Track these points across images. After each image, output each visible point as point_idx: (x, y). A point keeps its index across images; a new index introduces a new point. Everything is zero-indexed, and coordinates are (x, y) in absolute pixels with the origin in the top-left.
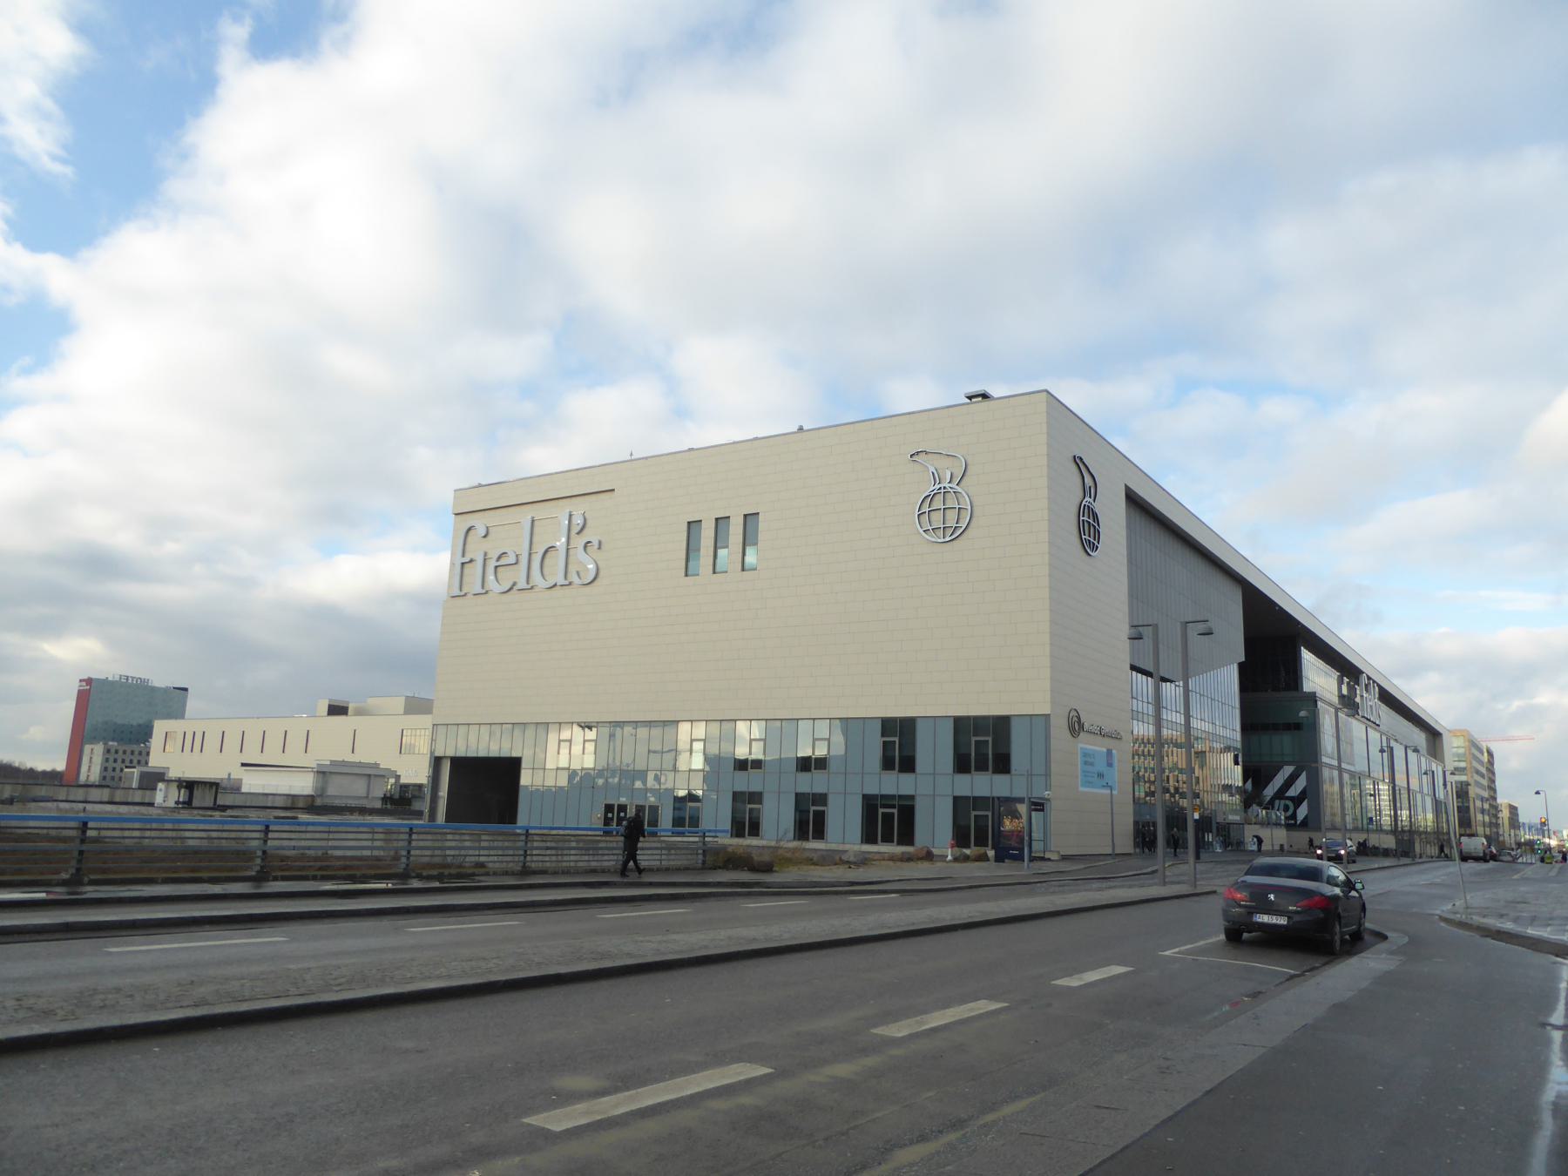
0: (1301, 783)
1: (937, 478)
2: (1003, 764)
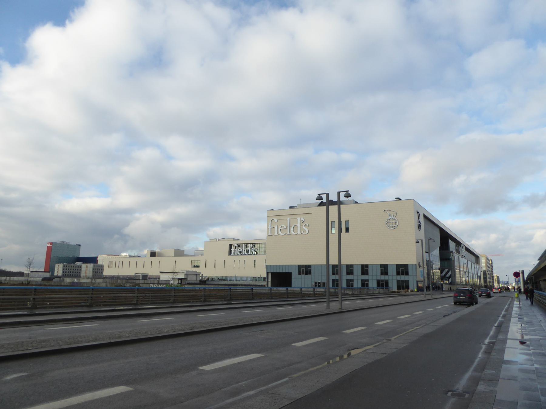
0: (450, 273)
1: (390, 216)
2: (407, 274)
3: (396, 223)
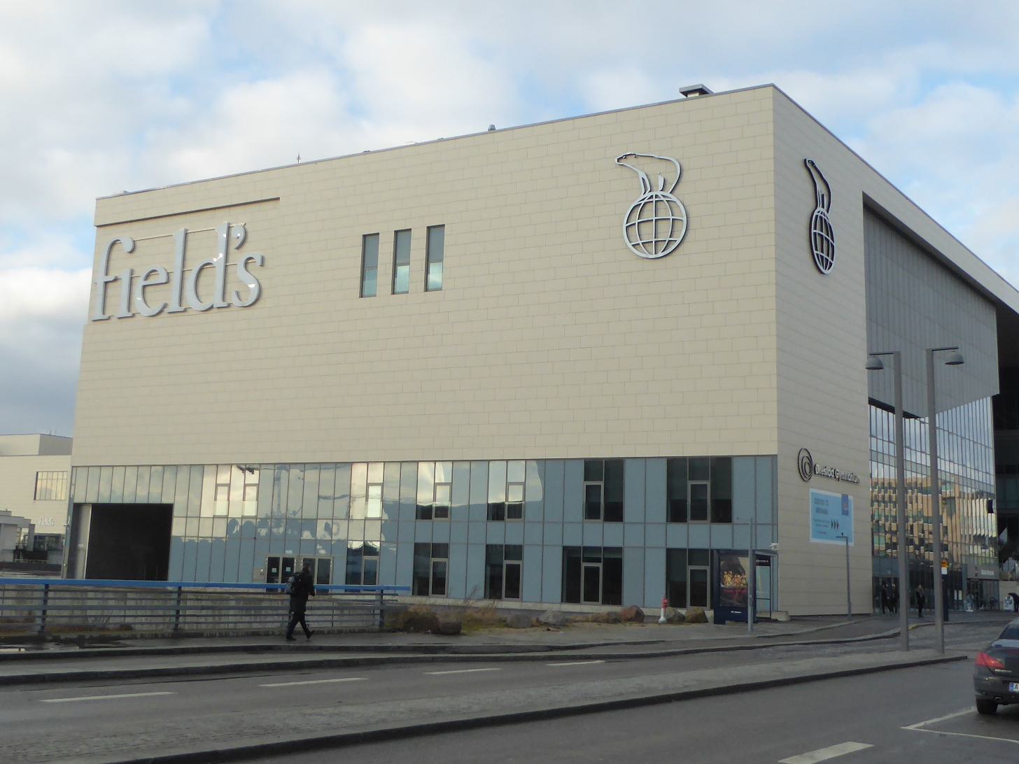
1: (648, 185)
3: (677, 224)
